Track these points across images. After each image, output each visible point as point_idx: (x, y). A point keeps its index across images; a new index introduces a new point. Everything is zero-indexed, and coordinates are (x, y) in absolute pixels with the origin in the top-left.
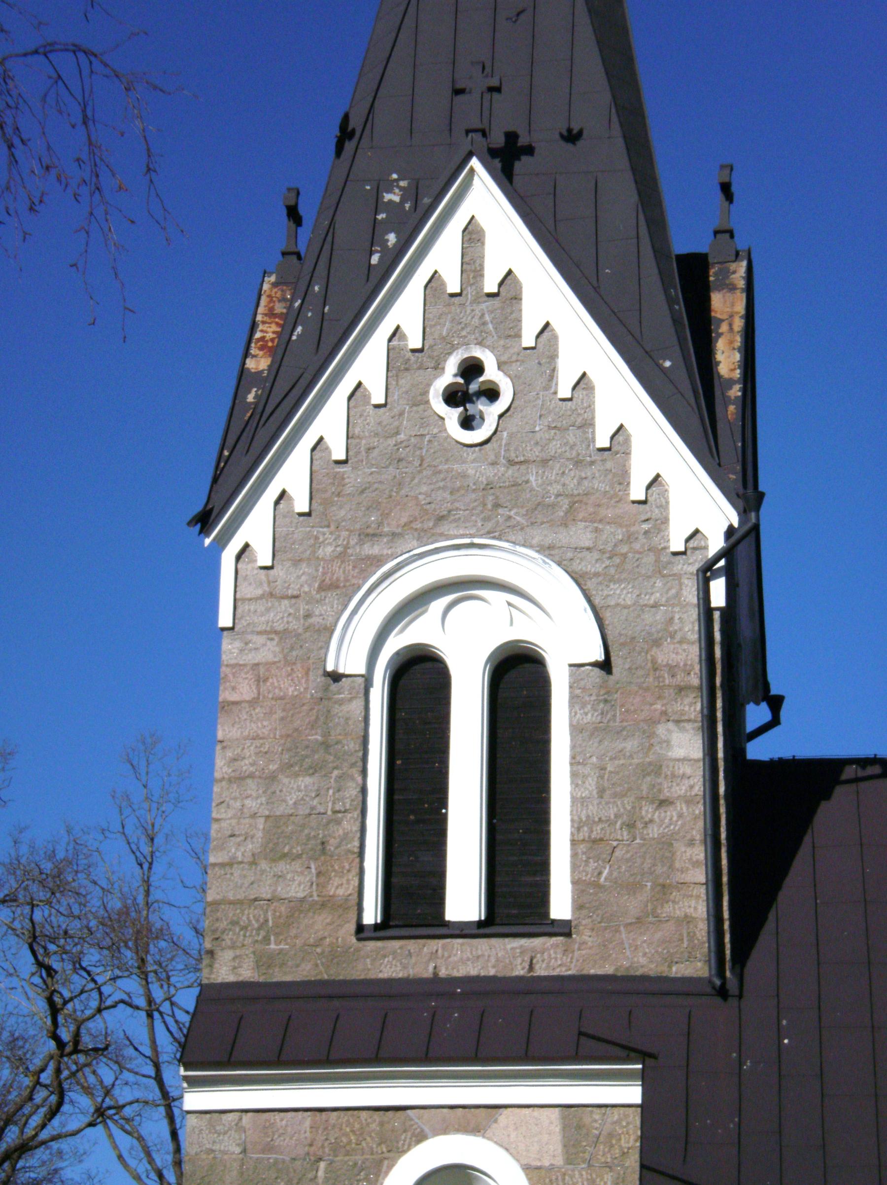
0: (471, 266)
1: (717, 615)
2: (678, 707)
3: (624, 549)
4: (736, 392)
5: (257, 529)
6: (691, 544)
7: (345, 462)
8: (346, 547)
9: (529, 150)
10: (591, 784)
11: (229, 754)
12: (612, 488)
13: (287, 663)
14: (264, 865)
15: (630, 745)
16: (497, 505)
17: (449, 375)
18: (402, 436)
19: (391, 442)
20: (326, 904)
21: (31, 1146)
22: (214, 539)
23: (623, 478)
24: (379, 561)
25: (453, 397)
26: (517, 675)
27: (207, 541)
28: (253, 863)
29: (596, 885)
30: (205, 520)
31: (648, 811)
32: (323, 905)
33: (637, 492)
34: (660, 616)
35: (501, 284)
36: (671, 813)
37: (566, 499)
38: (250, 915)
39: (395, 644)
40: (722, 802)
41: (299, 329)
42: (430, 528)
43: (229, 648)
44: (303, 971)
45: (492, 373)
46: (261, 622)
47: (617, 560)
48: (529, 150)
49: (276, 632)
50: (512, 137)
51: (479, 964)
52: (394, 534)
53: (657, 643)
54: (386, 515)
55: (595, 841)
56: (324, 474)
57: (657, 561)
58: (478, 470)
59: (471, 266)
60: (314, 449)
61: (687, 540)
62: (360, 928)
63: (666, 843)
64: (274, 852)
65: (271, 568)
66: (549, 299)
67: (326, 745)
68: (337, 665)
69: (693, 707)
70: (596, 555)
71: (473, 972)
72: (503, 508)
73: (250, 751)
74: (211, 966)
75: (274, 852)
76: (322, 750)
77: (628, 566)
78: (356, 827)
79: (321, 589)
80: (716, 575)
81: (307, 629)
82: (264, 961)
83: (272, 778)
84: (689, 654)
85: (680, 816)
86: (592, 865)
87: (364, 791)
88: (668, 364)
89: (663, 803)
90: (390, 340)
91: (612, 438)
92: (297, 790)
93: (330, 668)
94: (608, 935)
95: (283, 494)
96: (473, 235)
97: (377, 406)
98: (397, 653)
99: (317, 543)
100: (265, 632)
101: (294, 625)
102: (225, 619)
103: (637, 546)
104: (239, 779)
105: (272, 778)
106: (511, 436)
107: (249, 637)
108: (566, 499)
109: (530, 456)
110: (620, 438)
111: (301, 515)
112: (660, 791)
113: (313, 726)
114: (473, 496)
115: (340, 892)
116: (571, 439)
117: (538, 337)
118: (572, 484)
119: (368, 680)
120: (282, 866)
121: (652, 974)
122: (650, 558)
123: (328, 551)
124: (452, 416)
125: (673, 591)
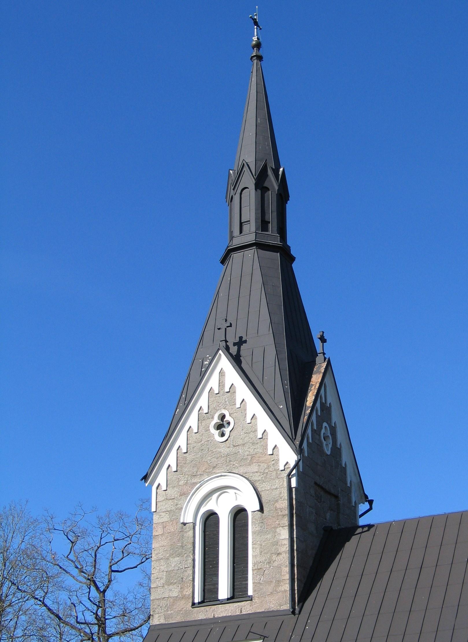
0: (221, 384)
1: (294, 489)
2: (283, 522)
3: (267, 471)
4: (308, 411)
5: (161, 479)
6: (286, 467)
7: (187, 453)
8: (187, 481)
9: (245, 342)
10: (258, 551)
11: (156, 552)
12: (263, 451)
13: (171, 521)
14: (166, 587)
15: (269, 536)
16: (230, 461)
17: (216, 420)
18: (203, 442)
19: (200, 444)
20: (184, 597)
22: (149, 483)
23: (266, 447)
24: (196, 484)
27: (147, 485)
28: (163, 586)
29: (259, 583)
30: (145, 478)
31: (274, 557)
32: (183, 598)
33: (270, 452)
34: (278, 492)
35: (230, 389)
36: (281, 557)
37: (247, 458)
38: (163, 603)
40: (295, 552)
41: (178, 410)
42: (211, 470)
43: (155, 517)
44: (177, 619)
45: (228, 418)
47: (265, 475)
48: (245, 342)
49: (168, 511)
50: (241, 338)
51: (226, 612)
52: (201, 474)
53: (277, 501)
54: (198, 469)
55: (259, 569)
57: (277, 473)
58: (224, 450)
60: (178, 450)
61: (285, 466)
62: (193, 604)
63: (279, 567)
64: (169, 583)
65: (166, 490)
66: (243, 392)
67: (182, 547)
68: (184, 520)
69: (286, 521)
70: (259, 474)
71: (225, 615)
72: (231, 464)
74: (153, 620)
75: (169, 583)
76: (178, 549)
77: (268, 476)
78: (191, 572)
79: (181, 495)
80: (293, 476)
81: (176, 509)
83: (168, 559)
84: (284, 504)
85: (283, 558)
86: (258, 577)
87: (194, 560)
88: (281, 407)
89: (279, 554)
90: (199, 411)
91: (263, 434)
92: (175, 561)
93: (182, 521)
94: (263, 599)
95: (169, 466)
96: (222, 373)
97: (196, 433)
98: (204, 513)
99: (179, 480)
100: (165, 512)
101: (173, 508)
102: (153, 509)
103: (271, 469)
104: (159, 560)
105: (168, 559)
106: (234, 438)
107: (161, 514)
108: (247, 458)
109: (239, 443)
110: (265, 434)
111: (174, 472)
112: (278, 550)
113: (179, 540)
114: (223, 459)
115: (187, 593)
116: (251, 436)
117: (241, 404)
118: (252, 451)
119: (194, 524)
120: (171, 587)
121: (275, 610)
122: (274, 473)
123: (181, 483)
125: (281, 483)
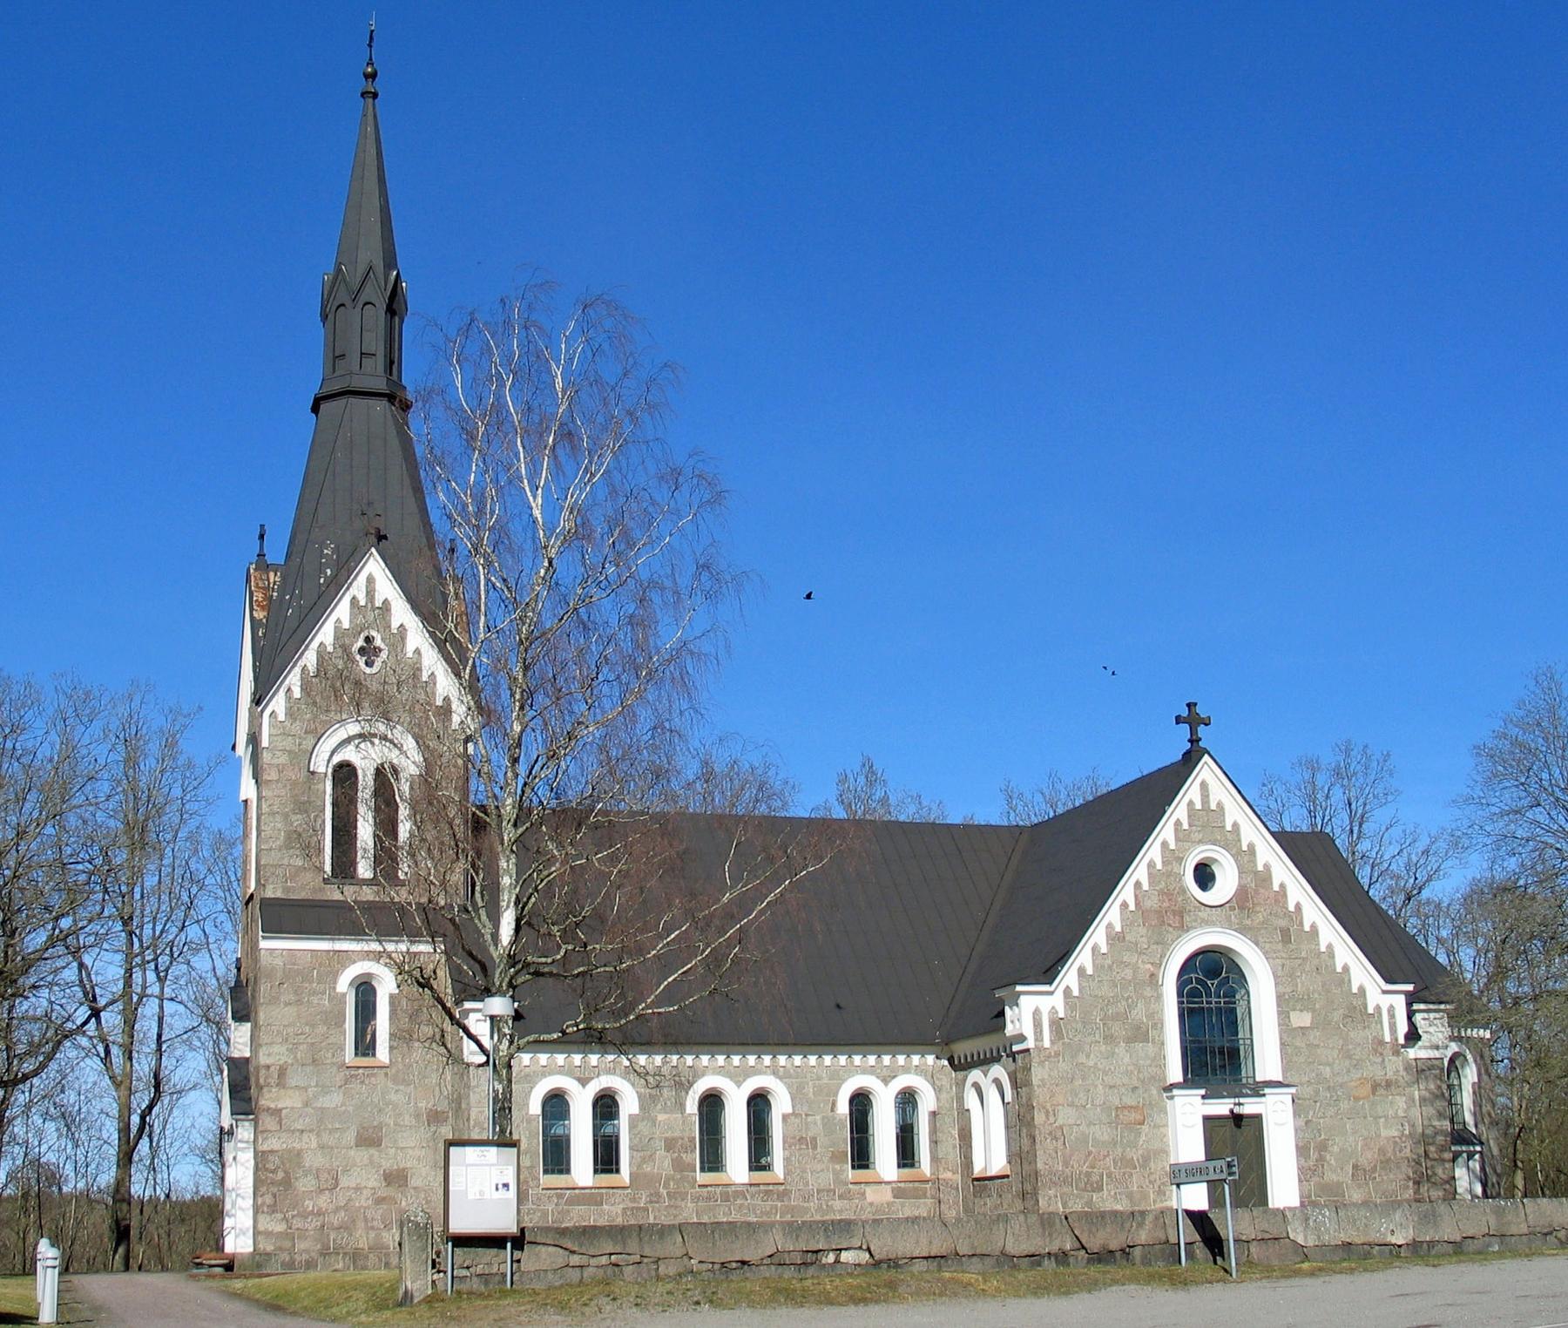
0: (370, 593)
17: (361, 643)
21: (124, 1074)
25: (362, 651)
26: (384, 778)
38: (279, 871)
39: (336, 759)
45: (378, 642)
46: (280, 745)
56: (1114, 938)
59: (370, 593)
73: (277, 801)
82: (286, 890)
96: (370, 580)
104: (273, 814)
124: (361, 661)
